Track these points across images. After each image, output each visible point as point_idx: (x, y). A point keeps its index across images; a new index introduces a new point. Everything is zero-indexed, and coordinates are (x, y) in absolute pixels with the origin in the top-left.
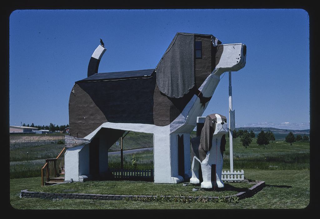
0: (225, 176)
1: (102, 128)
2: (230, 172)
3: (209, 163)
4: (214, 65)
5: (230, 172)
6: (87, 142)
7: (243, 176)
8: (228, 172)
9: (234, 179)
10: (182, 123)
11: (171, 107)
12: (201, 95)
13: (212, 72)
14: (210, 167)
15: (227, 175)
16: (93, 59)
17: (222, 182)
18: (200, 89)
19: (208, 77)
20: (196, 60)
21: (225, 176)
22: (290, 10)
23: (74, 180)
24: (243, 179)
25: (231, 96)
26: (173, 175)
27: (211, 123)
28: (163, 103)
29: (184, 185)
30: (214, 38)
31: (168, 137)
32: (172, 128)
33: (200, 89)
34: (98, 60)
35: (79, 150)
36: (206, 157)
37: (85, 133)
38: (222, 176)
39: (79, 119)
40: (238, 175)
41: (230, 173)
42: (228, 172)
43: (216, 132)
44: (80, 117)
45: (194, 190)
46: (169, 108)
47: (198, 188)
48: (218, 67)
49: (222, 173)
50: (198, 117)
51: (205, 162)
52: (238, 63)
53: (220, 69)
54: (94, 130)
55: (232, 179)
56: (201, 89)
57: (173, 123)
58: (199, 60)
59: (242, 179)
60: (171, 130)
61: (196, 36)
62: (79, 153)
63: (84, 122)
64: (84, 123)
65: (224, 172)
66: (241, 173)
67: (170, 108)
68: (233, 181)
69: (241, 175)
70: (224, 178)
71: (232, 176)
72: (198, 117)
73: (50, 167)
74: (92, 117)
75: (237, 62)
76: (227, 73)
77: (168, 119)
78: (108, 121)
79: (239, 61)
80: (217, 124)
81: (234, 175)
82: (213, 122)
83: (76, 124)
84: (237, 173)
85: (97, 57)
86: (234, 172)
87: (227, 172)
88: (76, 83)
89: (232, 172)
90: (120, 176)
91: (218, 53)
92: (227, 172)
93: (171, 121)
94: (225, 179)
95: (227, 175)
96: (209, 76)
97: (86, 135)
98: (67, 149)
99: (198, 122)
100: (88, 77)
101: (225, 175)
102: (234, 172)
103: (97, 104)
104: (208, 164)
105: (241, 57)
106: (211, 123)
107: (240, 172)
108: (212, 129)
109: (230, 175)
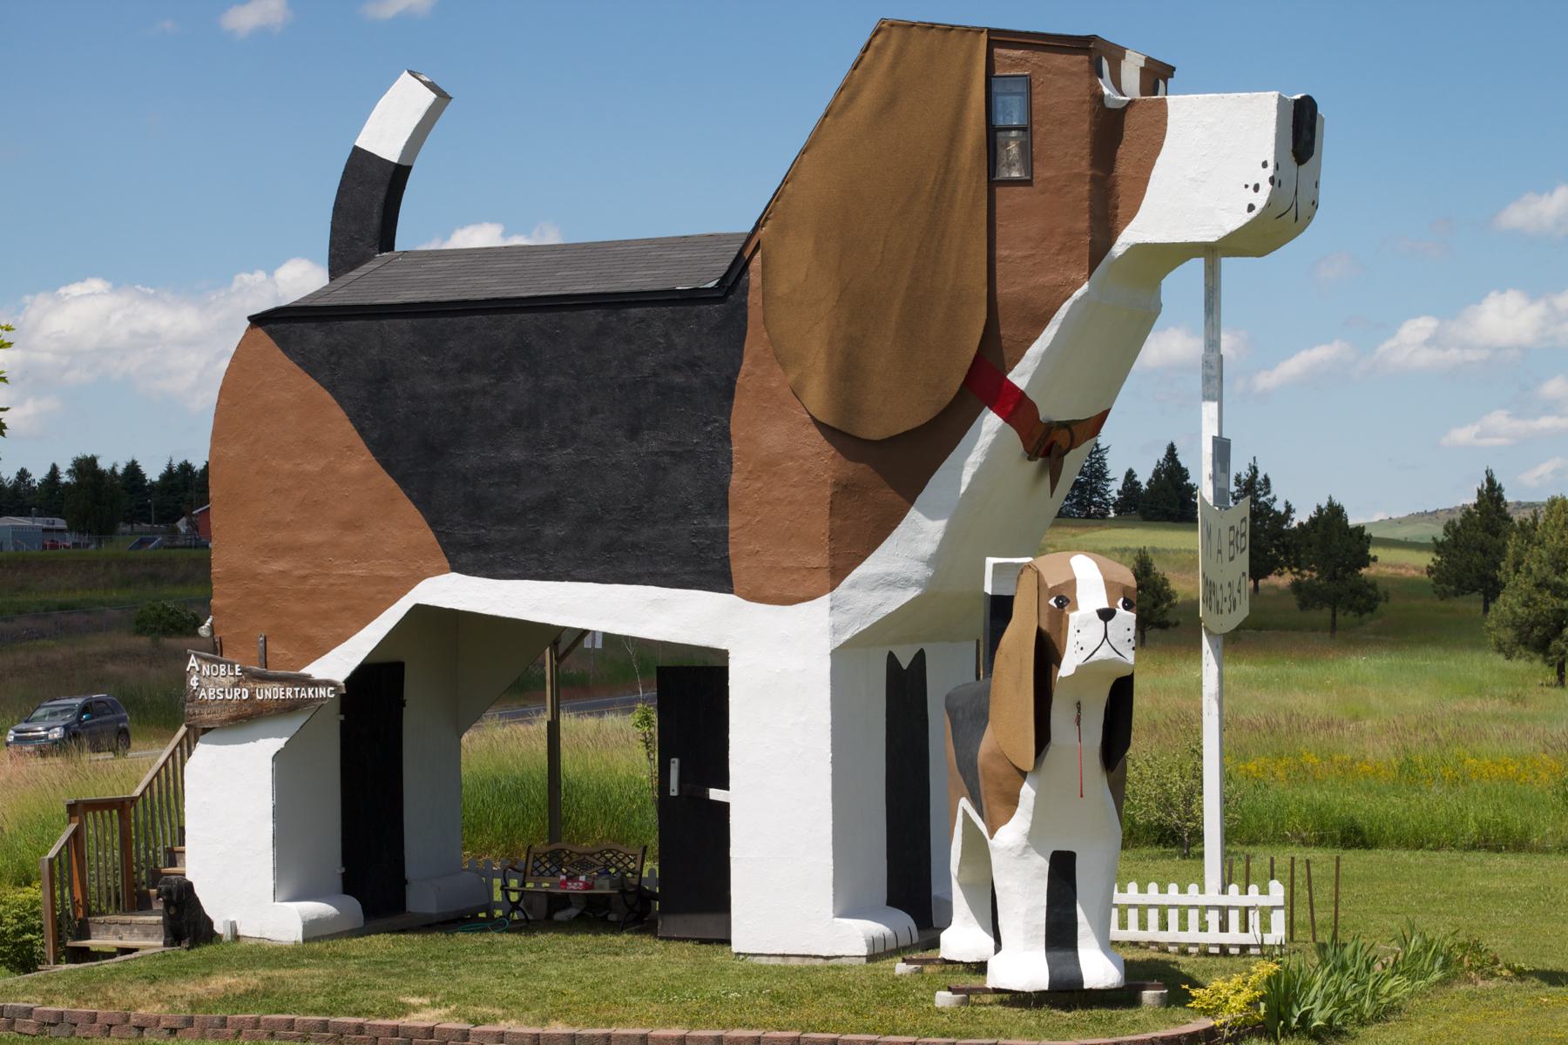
0: (1133, 915)
1: (419, 611)
2: (1202, 890)
3: (1034, 838)
4: (1106, 221)
5: (1202, 890)
6: (322, 692)
7: (1279, 920)
8: (1193, 896)
9: (1225, 939)
10: (906, 583)
11: (836, 484)
12: (1015, 406)
13: (1090, 273)
14: (1042, 864)
15: (1163, 911)
16: (360, 161)
17: (1111, 946)
18: (1020, 377)
19: (1066, 306)
20: (999, 191)
21: (1133, 915)
22: (829, 734)
23: (241, 932)
24: (1278, 933)
25: (1215, 405)
26: (849, 907)
27: (1045, 612)
28: (792, 458)
29: (901, 968)
30: (1117, 54)
31: (823, 668)
32: (842, 618)
33: (1020, 377)
34: (397, 166)
35: (278, 743)
36: (1018, 809)
37: (308, 640)
38: (1115, 912)
39: (275, 551)
40: (1170, 912)
41: (1203, 900)
42: (1193, 896)
43: (1067, 668)
44: (280, 536)
45: (944, 998)
46: (828, 493)
47: (969, 991)
48: (1130, 236)
49: (1118, 898)
50: (991, 561)
51: (1010, 836)
52: (1254, 214)
53: (1139, 250)
54: (367, 623)
55: (1214, 936)
56: (1021, 375)
57: (853, 586)
58: (1017, 195)
59: (1130, 930)
60: (835, 630)
61: (998, 39)
62: (277, 757)
63: (303, 572)
64: (305, 578)
65: (1123, 890)
66: (1264, 901)
67: (833, 494)
68: (1216, 950)
69: (1266, 913)
70: (1123, 925)
71: (1213, 917)
72: (991, 561)
73: (90, 849)
74: (351, 539)
75: (1251, 208)
76: (1197, 265)
77: (820, 559)
78: (455, 569)
79: (1260, 200)
80: (1074, 618)
81: (1224, 911)
82: (1052, 602)
83: (254, 577)
84: (1244, 901)
85: (390, 150)
86: (1224, 891)
87: (1183, 890)
88: (257, 320)
89: (1213, 896)
90: (515, 906)
91: (1126, 155)
92: (1183, 890)
93: (837, 574)
94: (1133, 933)
95: (1183, 912)
96: (1078, 294)
97: (318, 650)
98: (198, 732)
99: (988, 589)
100: (331, 280)
101: (1253, 908)
102: (1224, 891)
103: (384, 451)
104: (1027, 847)
105: (1272, 180)
106: (1042, 610)
107: (1264, 891)
108: (1047, 652)
109: (1204, 909)
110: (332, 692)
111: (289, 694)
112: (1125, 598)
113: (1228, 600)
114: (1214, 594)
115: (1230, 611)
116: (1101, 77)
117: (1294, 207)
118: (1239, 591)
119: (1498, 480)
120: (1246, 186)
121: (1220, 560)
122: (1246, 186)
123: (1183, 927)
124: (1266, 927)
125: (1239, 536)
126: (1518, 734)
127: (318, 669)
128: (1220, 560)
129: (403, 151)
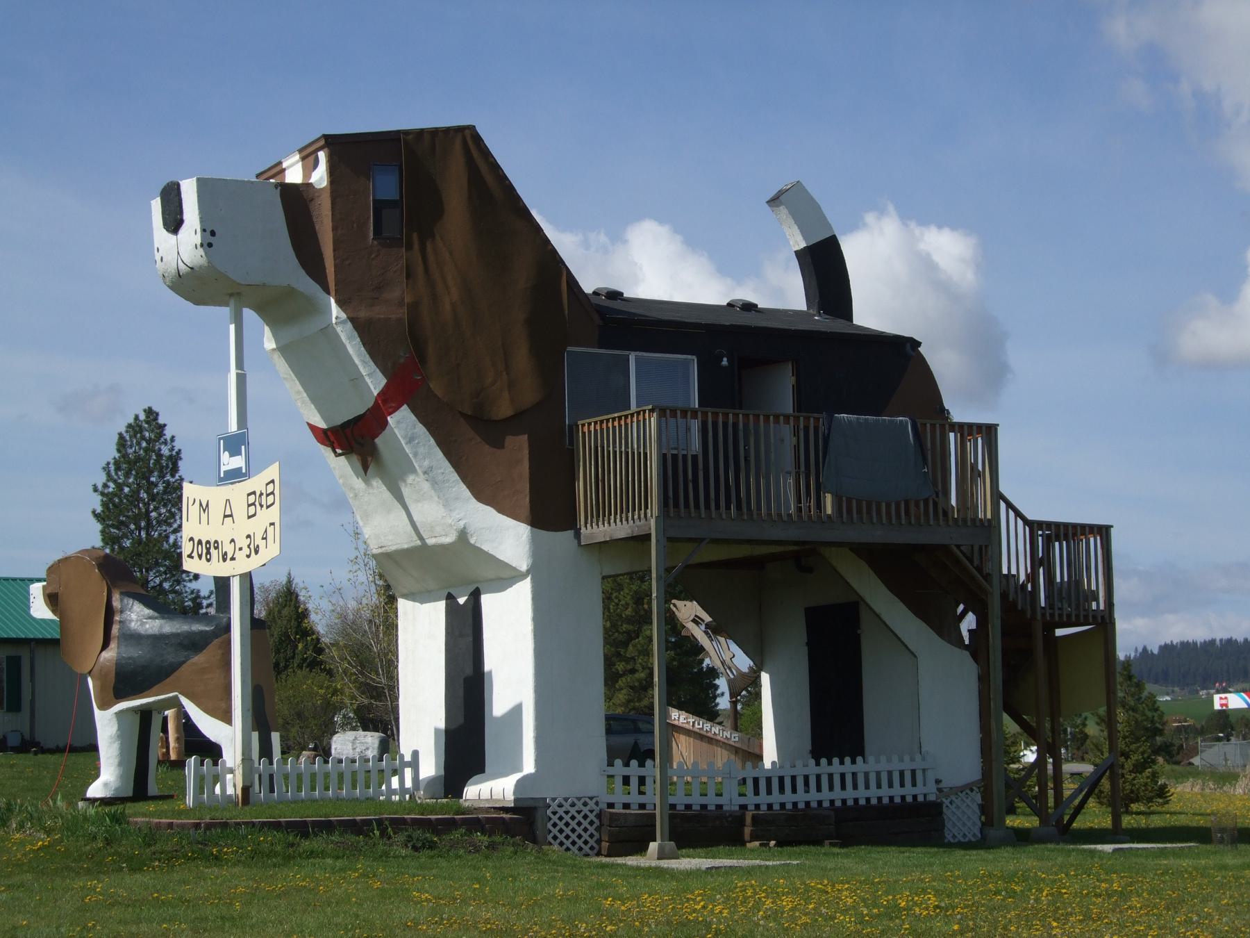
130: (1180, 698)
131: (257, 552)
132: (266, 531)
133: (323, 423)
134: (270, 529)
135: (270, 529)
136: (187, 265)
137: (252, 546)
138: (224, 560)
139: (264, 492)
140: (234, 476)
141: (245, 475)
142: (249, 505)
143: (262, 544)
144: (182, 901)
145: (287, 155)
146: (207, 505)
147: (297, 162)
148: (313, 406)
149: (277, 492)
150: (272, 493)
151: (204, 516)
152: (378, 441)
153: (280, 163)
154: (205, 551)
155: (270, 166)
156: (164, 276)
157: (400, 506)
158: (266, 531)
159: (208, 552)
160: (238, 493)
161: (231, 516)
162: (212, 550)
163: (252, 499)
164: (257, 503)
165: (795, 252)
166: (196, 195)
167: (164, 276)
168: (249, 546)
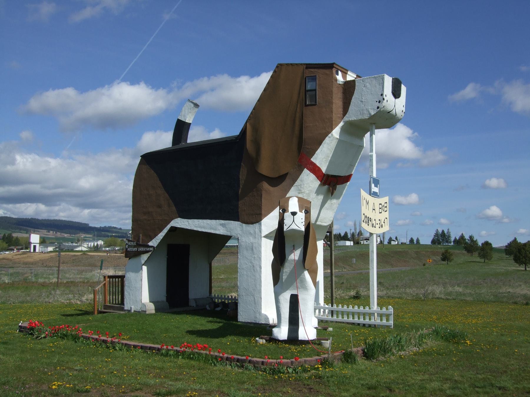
1: (172, 227)
7: (392, 318)
97: (151, 239)
110: (153, 249)
111: (148, 249)
112: (305, 210)
113: (379, 224)
114: (371, 221)
115: (380, 228)
116: (338, 75)
117: (394, 108)
118: (384, 223)
119: (450, 231)
120: (377, 102)
121: (367, 208)
122: (377, 102)
123: (359, 318)
124: (388, 320)
125: (384, 207)
126: (245, 272)
127: (150, 244)
128: (367, 208)
129: (189, 129)
130: (222, 276)
131: (382, 227)
132: (385, 220)
133: (325, 171)
134: (386, 220)
135: (386, 220)
136: (396, 113)
137: (380, 224)
138: (373, 227)
139: (384, 205)
140: (375, 195)
141: (378, 196)
142: (380, 208)
143: (383, 224)
144: (227, 391)
145: (353, 71)
146: (368, 202)
147: (353, 77)
148: (328, 164)
149: (388, 207)
150: (386, 207)
151: (367, 206)
152: (338, 186)
153: (347, 71)
154: (367, 221)
155: (344, 67)
156: (384, 106)
157: (319, 209)
158: (385, 220)
159: (368, 222)
160: (377, 201)
161: (374, 210)
162: (369, 221)
163: (381, 206)
164: (382, 208)
165: (178, 119)
166: (391, 86)
167: (384, 106)
168: (380, 224)
